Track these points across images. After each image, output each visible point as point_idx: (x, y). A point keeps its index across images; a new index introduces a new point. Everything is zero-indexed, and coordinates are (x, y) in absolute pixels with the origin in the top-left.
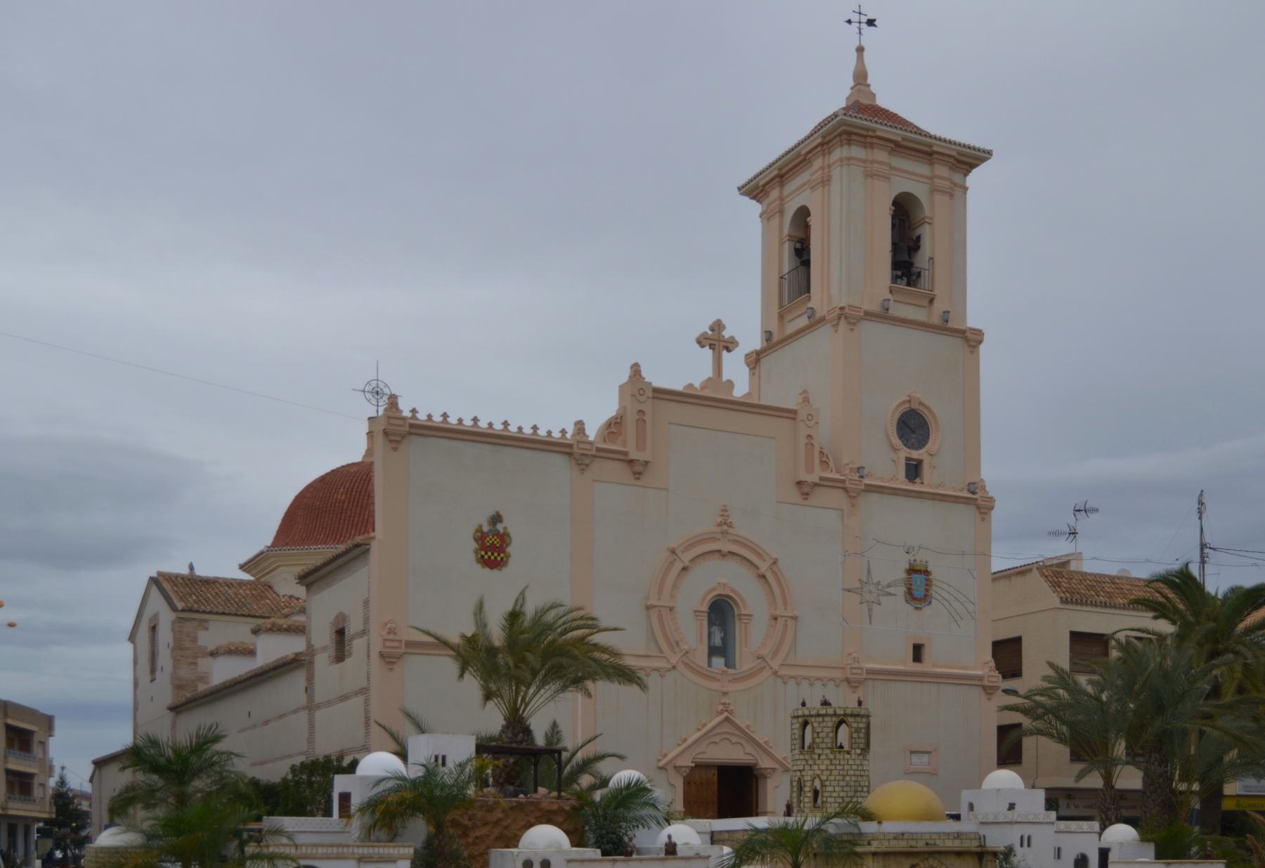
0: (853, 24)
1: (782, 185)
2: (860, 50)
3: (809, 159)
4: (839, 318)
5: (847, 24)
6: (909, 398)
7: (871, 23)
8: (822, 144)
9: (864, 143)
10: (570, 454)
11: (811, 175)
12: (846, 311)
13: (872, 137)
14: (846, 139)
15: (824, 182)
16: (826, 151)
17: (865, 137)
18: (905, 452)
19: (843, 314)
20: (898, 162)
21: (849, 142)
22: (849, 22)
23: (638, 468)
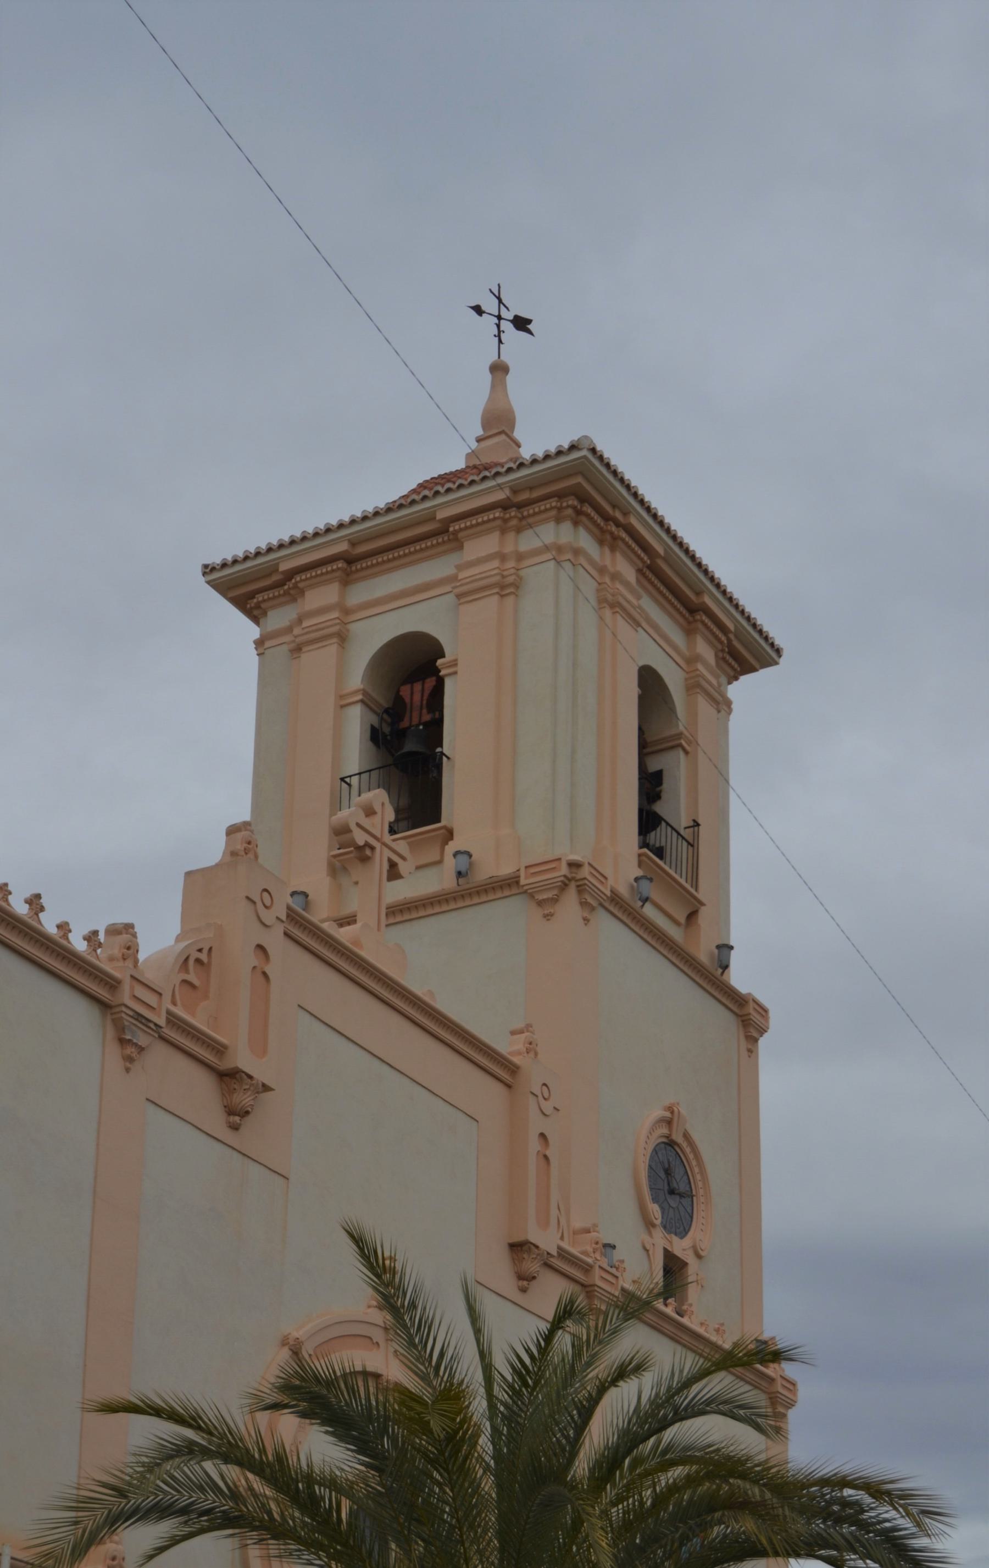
0: (484, 315)
1: (347, 580)
2: (499, 369)
3: (455, 533)
4: (564, 886)
5: (473, 313)
6: (668, 1114)
7: (521, 324)
8: (504, 506)
9: (603, 531)
10: (104, 1006)
11: (460, 568)
12: (585, 872)
13: (618, 524)
14: (574, 508)
15: (503, 587)
16: (514, 522)
17: (607, 518)
18: (660, 1240)
19: (573, 879)
20: (361, 593)
21: (578, 518)
22: (478, 310)
23: (243, 1099)
